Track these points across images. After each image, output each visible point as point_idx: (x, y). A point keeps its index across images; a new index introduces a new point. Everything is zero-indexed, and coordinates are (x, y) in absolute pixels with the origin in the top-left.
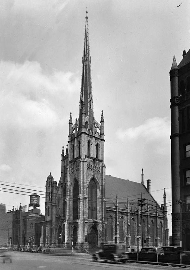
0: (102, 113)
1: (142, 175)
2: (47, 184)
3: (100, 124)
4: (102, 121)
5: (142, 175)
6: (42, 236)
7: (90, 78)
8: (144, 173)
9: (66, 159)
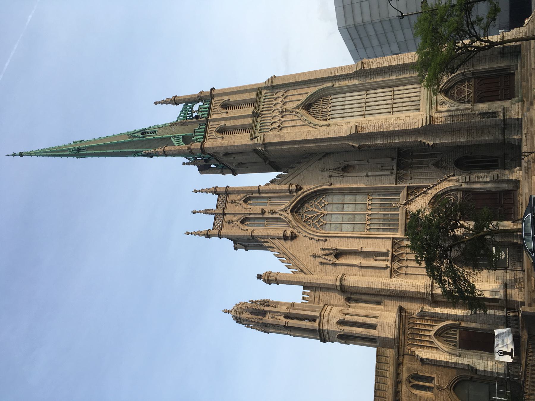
3: (181, 106)
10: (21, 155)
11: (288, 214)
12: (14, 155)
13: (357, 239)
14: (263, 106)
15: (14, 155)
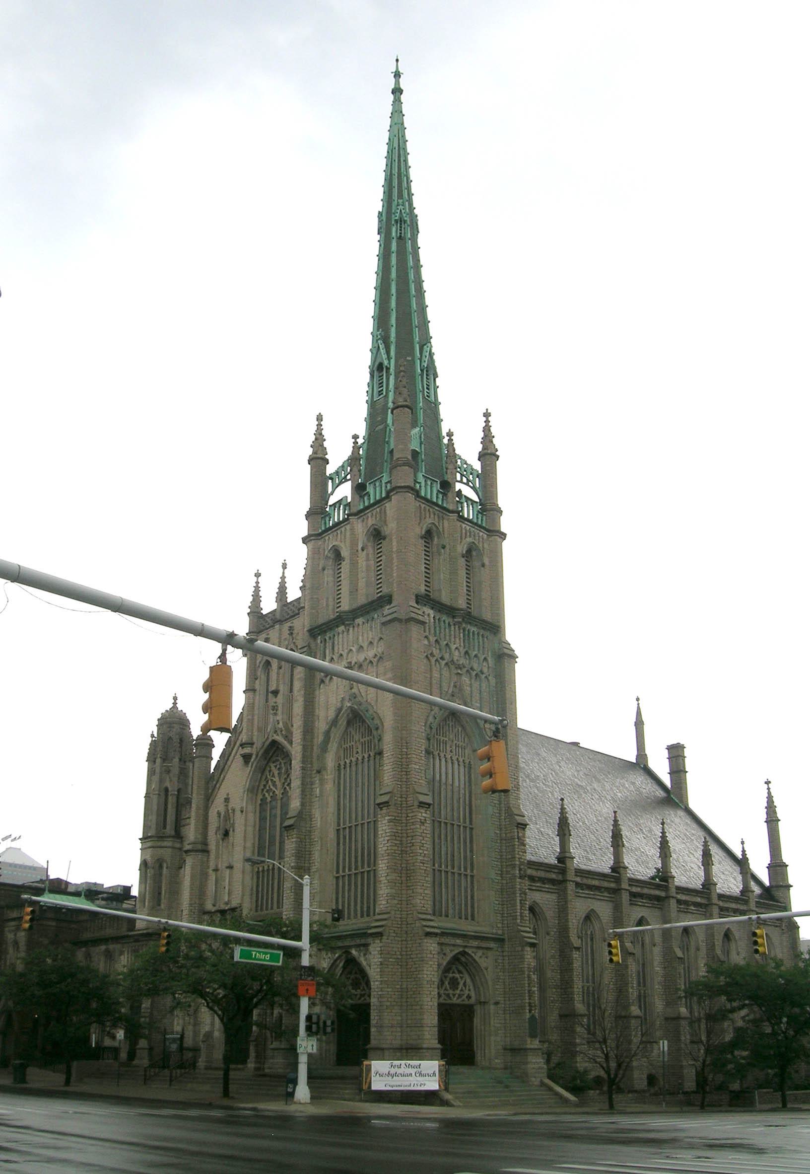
0: (487, 422)
1: (639, 724)
2: (153, 745)
3: (477, 466)
4: (489, 455)
5: (639, 724)
6: (365, 931)
7: (417, 266)
8: (644, 718)
9: (277, 626)
10: (397, 91)
11: (364, 989)
12: (397, 75)
13: (93, 1162)
14: (439, 619)
15: (397, 75)
